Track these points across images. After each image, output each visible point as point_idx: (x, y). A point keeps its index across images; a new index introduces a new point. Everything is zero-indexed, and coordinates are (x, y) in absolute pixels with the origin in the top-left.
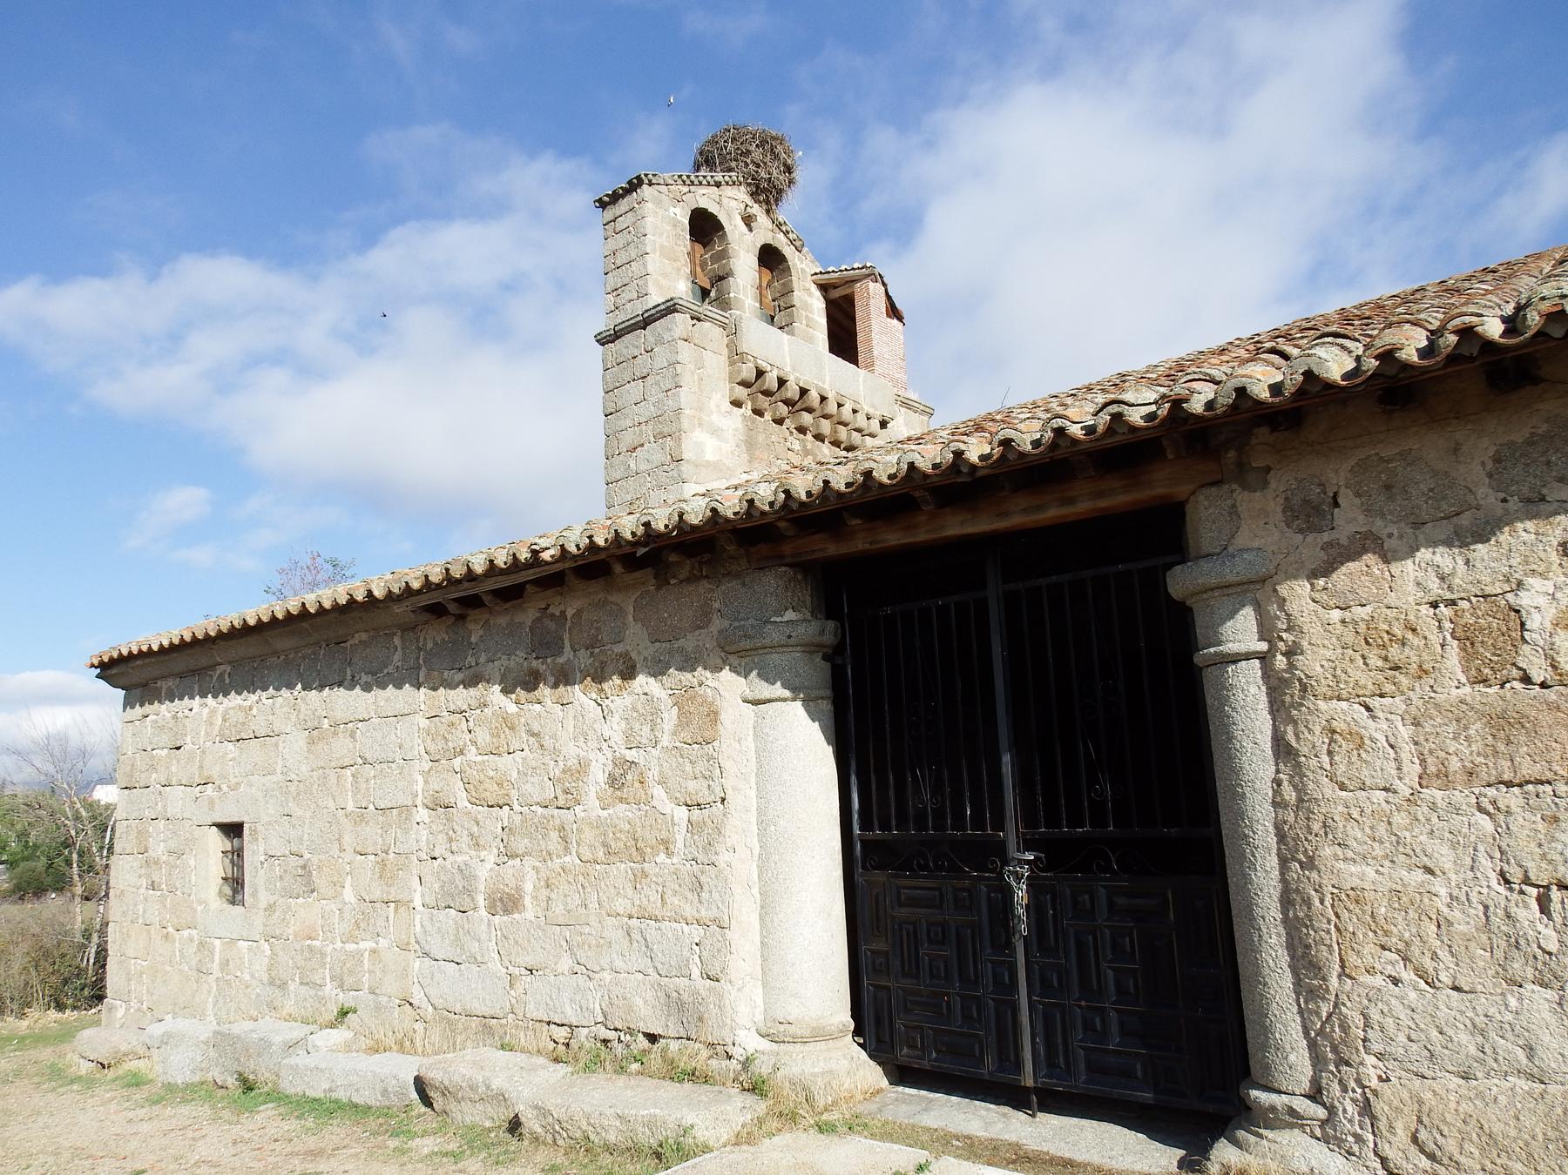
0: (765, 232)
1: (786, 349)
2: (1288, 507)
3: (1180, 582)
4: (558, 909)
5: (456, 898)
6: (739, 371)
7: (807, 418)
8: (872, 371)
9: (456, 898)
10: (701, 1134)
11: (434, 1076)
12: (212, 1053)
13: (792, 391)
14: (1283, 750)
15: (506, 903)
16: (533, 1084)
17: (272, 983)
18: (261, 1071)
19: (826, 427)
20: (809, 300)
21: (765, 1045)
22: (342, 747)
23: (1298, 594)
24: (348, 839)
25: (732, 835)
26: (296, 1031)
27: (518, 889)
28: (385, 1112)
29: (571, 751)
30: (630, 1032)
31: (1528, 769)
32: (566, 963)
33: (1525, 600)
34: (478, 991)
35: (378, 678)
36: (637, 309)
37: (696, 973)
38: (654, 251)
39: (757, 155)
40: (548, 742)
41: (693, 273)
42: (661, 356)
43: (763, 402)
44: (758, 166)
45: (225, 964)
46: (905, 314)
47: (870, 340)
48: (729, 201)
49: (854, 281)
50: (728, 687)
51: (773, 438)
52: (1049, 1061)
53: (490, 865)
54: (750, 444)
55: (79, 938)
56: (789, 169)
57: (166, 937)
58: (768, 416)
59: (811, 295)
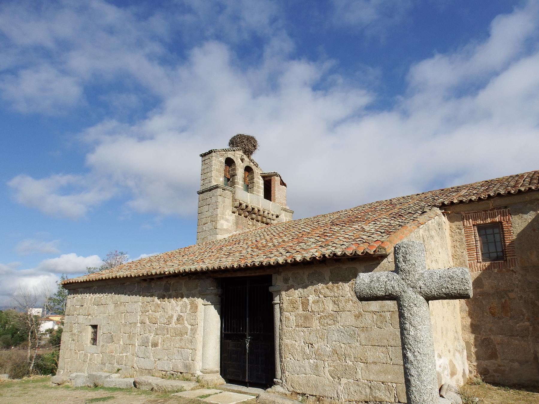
0: (247, 162)
2: (283, 279)
3: (271, 289)
4: (165, 346)
5: (145, 343)
7: (254, 216)
9: (145, 343)
10: (185, 388)
11: (137, 380)
12: (88, 379)
13: (250, 209)
14: (281, 320)
15: (155, 345)
16: (155, 381)
17: (102, 364)
18: (99, 382)
19: (259, 218)
21: (201, 374)
22: (122, 308)
23: (283, 293)
24: (122, 330)
25: (198, 332)
26: (108, 374)
27: (158, 342)
28: (127, 389)
29: (170, 312)
30: (177, 372)
31: (308, 325)
32: (166, 358)
33: (309, 298)
34: (147, 364)
35: (131, 293)
36: (208, 186)
37: (190, 359)
40: (166, 310)
41: (225, 175)
42: (214, 200)
43: (241, 212)
45: (90, 359)
48: (237, 155)
50: (200, 302)
52: (250, 377)
53: (152, 336)
54: (237, 223)
55: (29, 361)
56: (255, 146)
57: (76, 353)
58: (243, 215)
59: (259, 179)
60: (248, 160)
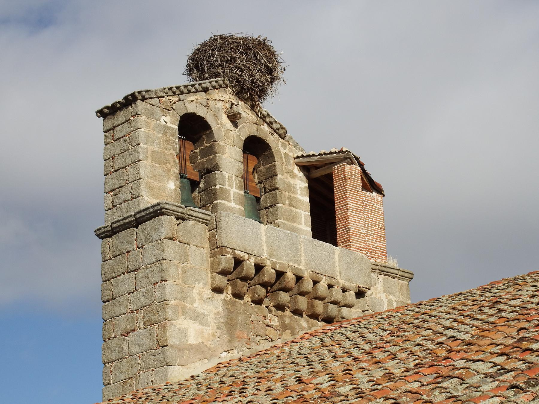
0: (249, 125)
1: (263, 238)
6: (219, 263)
7: (284, 297)
8: (348, 247)
13: (269, 274)
19: (303, 303)
20: (292, 181)
36: (130, 210)
38: (146, 158)
39: (241, 60)
42: (150, 257)
43: (242, 286)
44: (242, 71)
46: (384, 187)
47: (346, 218)
48: (216, 105)
49: (333, 163)
51: (253, 317)
54: (230, 325)
58: (247, 298)
59: (293, 176)
60: (254, 118)
